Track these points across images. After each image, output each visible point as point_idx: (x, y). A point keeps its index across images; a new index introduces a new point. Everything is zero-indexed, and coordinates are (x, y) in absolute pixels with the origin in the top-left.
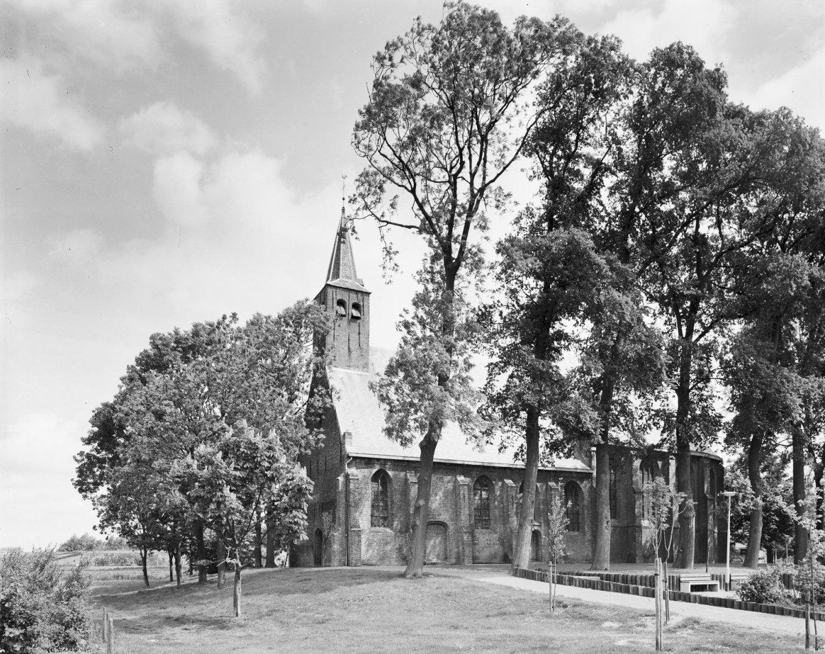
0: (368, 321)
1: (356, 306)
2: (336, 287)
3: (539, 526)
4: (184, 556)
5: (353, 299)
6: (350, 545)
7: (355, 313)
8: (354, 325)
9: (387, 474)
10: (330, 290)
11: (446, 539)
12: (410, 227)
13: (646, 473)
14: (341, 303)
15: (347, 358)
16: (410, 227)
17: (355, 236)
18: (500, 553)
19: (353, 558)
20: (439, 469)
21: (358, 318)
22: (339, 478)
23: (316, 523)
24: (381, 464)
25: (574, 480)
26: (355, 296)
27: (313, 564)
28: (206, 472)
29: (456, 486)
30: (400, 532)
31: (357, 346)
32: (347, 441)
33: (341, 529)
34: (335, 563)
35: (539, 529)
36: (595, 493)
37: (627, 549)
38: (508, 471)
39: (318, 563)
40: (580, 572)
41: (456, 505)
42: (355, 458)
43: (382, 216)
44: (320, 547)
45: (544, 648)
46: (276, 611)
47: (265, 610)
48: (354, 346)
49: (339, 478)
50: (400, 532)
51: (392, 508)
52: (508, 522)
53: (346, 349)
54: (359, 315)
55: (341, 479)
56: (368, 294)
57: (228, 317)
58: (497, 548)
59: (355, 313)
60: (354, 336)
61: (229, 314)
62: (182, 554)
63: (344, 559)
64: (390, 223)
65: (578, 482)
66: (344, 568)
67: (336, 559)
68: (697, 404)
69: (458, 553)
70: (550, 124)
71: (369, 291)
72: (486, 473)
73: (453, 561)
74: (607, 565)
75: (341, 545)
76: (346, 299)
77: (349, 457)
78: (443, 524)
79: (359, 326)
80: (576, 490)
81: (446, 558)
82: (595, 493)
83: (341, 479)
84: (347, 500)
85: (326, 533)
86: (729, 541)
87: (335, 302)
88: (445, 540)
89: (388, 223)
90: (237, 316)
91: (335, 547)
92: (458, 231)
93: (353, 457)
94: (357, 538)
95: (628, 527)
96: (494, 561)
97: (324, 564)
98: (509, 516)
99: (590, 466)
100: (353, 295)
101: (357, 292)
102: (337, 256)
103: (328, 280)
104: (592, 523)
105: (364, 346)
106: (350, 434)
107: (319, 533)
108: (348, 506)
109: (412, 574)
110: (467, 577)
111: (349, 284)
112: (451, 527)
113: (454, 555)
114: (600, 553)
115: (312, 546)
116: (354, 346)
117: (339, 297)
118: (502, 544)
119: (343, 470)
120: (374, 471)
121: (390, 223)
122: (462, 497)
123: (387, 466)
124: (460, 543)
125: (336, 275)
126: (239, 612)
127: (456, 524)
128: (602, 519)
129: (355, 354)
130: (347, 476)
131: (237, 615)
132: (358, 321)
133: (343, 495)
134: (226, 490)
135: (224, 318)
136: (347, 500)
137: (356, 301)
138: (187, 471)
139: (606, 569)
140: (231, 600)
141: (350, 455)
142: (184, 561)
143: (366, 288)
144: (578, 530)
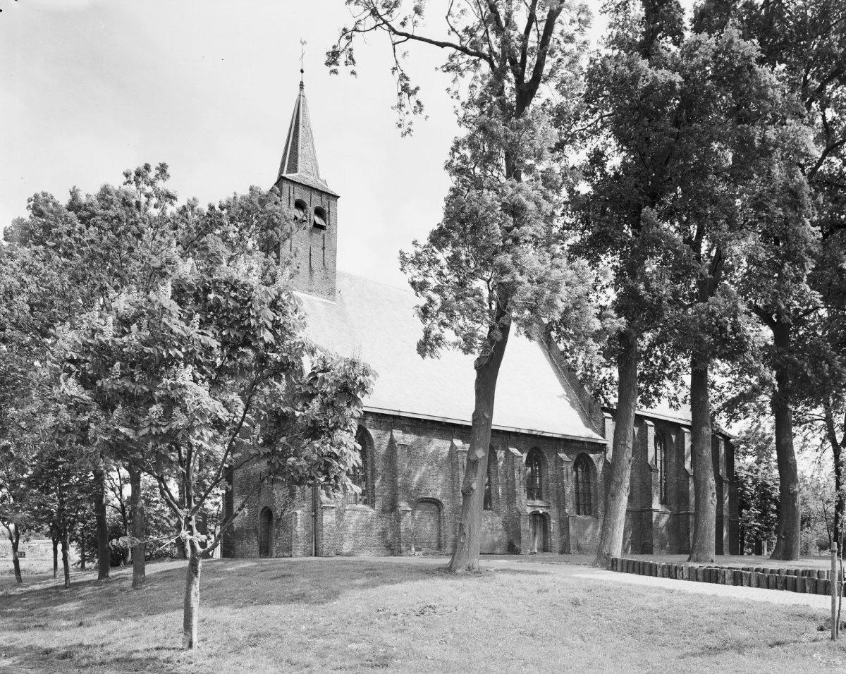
1: (319, 212)
2: (292, 181)
3: (547, 507)
4: (74, 543)
7: (319, 221)
10: (285, 185)
11: (439, 522)
12: (443, 45)
13: (658, 448)
14: (300, 205)
15: (307, 279)
16: (443, 45)
17: (351, 67)
19: (325, 544)
20: (432, 429)
21: (322, 227)
23: (262, 500)
25: (586, 452)
27: (258, 555)
28: (135, 336)
33: (307, 505)
34: (298, 553)
35: (548, 511)
36: (610, 468)
37: (545, 548)
38: (512, 437)
39: (265, 551)
40: (539, 570)
41: (452, 478)
43: (403, 24)
44: (268, 532)
46: (267, 635)
47: (241, 635)
48: (317, 264)
53: (307, 266)
54: (324, 224)
56: (338, 197)
57: (153, 168)
58: (499, 536)
59: (319, 221)
60: (317, 251)
61: (154, 165)
62: (71, 541)
63: (311, 547)
64: (413, 37)
66: (314, 558)
67: (300, 546)
71: (336, 192)
74: (712, 555)
75: (306, 527)
76: (307, 200)
78: (436, 503)
79: (323, 238)
80: (587, 465)
81: (439, 547)
82: (610, 468)
85: (278, 512)
87: (293, 202)
89: (409, 36)
90: (168, 171)
95: (642, 511)
96: (498, 551)
97: (275, 554)
98: (514, 494)
100: (316, 197)
101: (321, 193)
102: (293, 143)
103: (281, 171)
105: (330, 266)
107: (268, 513)
109: (465, 567)
111: (310, 181)
112: (447, 507)
114: (703, 537)
115: (256, 530)
116: (317, 264)
117: (298, 197)
118: (506, 528)
121: (413, 37)
123: (367, 422)
125: (293, 168)
126: (195, 639)
127: (452, 502)
128: (705, 489)
129: (318, 275)
131: (190, 646)
132: (323, 232)
134: (185, 374)
135: (147, 167)
137: (319, 205)
139: (712, 561)
140: (179, 616)
142: (74, 554)
143: (332, 188)
144: (590, 514)
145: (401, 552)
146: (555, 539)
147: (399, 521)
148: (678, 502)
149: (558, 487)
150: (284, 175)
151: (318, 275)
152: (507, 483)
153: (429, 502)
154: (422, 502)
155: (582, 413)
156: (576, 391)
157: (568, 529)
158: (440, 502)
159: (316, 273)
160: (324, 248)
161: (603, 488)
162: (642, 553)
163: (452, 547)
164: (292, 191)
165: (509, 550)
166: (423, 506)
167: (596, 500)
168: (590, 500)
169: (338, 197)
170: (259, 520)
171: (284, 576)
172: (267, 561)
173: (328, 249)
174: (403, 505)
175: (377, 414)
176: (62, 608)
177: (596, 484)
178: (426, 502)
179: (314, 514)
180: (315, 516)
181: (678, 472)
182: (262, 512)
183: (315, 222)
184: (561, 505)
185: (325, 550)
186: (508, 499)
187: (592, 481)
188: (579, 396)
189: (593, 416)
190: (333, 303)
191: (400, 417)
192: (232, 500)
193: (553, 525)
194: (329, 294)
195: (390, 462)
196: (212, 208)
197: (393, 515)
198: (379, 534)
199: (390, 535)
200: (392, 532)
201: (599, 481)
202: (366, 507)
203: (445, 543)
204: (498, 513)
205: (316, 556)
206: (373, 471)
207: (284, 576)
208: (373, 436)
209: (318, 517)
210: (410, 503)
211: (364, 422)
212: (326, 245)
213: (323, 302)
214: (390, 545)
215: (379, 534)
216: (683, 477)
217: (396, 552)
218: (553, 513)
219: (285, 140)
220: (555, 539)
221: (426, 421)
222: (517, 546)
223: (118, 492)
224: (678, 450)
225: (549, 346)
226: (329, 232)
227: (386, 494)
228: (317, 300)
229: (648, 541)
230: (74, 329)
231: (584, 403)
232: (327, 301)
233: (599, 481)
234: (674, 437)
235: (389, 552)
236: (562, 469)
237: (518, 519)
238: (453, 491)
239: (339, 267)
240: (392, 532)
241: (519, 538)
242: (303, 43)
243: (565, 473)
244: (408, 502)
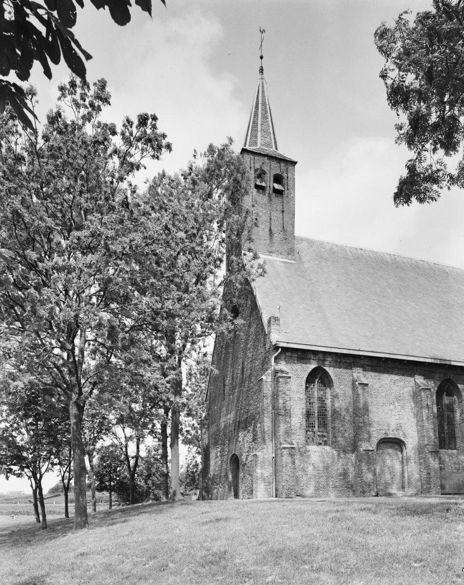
0: (294, 197)
1: (278, 179)
5: (272, 169)
6: (279, 468)
8: (276, 200)
15: (268, 241)
26: (277, 165)
31: (280, 228)
42: (285, 350)
44: (236, 477)
53: (267, 230)
54: (283, 189)
55: (267, 378)
56: (296, 163)
60: (276, 215)
68: (69, 140)
70: (406, 87)
72: (452, 376)
85: (244, 458)
92: (72, 508)
93: (283, 348)
100: (274, 164)
102: (254, 122)
105: (289, 229)
129: (277, 237)
138: (402, 132)
150: (247, 147)
151: (277, 237)
158: (403, 442)
159: (275, 235)
160: (283, 211)
164: (252, 162)
169: (296, 163)
170: (228, 466)
171: (218, 520)
172: (237, 500)
173: (288, 213)
175: (336, 354)
178: (388, 442)
182: (231, 459)
183: (274, 188)
191: (360, 356)
192: (209, 451)
196: (164, 136)
198: (340, 475)
205: (276, 497)
207: (218, 520)
212: (285, 209)
215: (340, 475)
219: (247, 126)
221: (387, 359)
223: (124, 449)
226: (287, 197)
228: (277, 260)
239: (297, 233)
242: (262, 32)
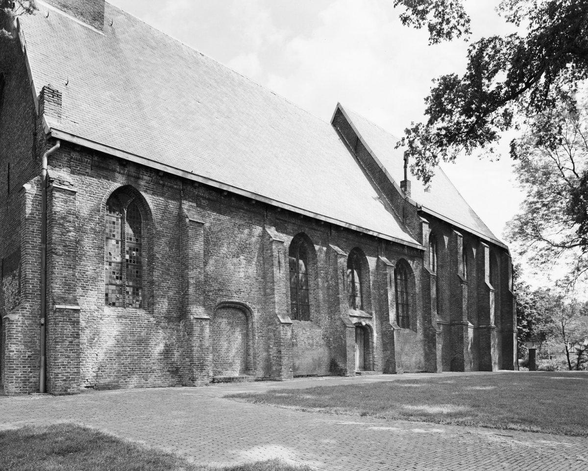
6: (51, 342)
9: (142, 199)
18: (326, 360)
20: (239, 208)
22: (27, 186)
24: (129, 176)
25: (405, 258)
29: (265, 243)
30: (168, 318)
32: (48, 106)
41: (264, 278)
42: (67, 146)
45: (64, 6)
49: (27, 186)
50: (168, 318)
51: (152, 270)
52: (338, 311)
55: (31, 189)
58: (322, 353)
65: (409, 261)
69: (268, 360)
73: (260, 373)
77: (54, 140)
78: (243, 309)
80: (406, 274)
83: (31, 189)
84: (46, 239)
86: (515, 343)
88: (247, 337)
91: (13, 348)
93: (63, 142)
94: (69, 329)
99: (419, 237)
104: (425, 312)
106: (55, 94)
108: (47, 253)
110: (309, 410)
113: (261, 364)
119: (37, 168)
120: (116, 185)
122: (276, 263)
123: (142, 183)
124: (272, 342)
130: (47, 187)
133: (35, 227)
136: (46, 239)
141: (55, 134)
144: (408, 327)
145: (193, 380)
146: (377, 355)
147: (190, 334)
148: (479, 317)
149: (380, 295)
152: (328, 288)
153: (234, 308)
154: (224, 307)
155: (396, 218)
156: (387, 195)
157: (392, 343)
158: (249, 309)
161: (421, 299)
162: (480, 371)
163: (264, 369)
165: (331, 370)
166: (225, 312)
167: (415, 311)
168: (407, 311)
174: (198, 311)
176: (224, 350)
177: (415, 294)
178: (229, 307)
179: (43, 321)
180: (45, 325)
181: (478, 286)
184: (383, 317)
185: (60, 383)
186: (329, 308)
187: (410, 291)
188: (391, 201)
189: (408, 221)
190: (100, 32)
193: (375, 337)
194: (95, 19)
195: (178, 247)
197: (182, 324)
199: (177, 354)
200: (181, 350)
201: (417, 290)
202: (141, 313)
203: (255, 363)
204: (318, 324)
206: (152, 258)
208: (151, 206)
209: (50, 327)
210: (208, 308)
211: (136, 182)
213: (81, 25)
214: (177, 369)
216: (483, 291)
217: (186, 380)
218: (374, 324)
220: (377, 355)
222: (341, 365)
224: (477, 264)
225: (356, 149)
227: (171, 293)
229: (458, 356)
230: (76, 300)
231: (397, 207)
232: (90, 27)
233: (417, 290)
234: (474, 250)
235: (175, 380)
236: (386, 274)
237: (343, 333)
238: (265, 295)
240: (181, 350)
241: (344, 356)
243: (388, 280)
244: (204, 306)
